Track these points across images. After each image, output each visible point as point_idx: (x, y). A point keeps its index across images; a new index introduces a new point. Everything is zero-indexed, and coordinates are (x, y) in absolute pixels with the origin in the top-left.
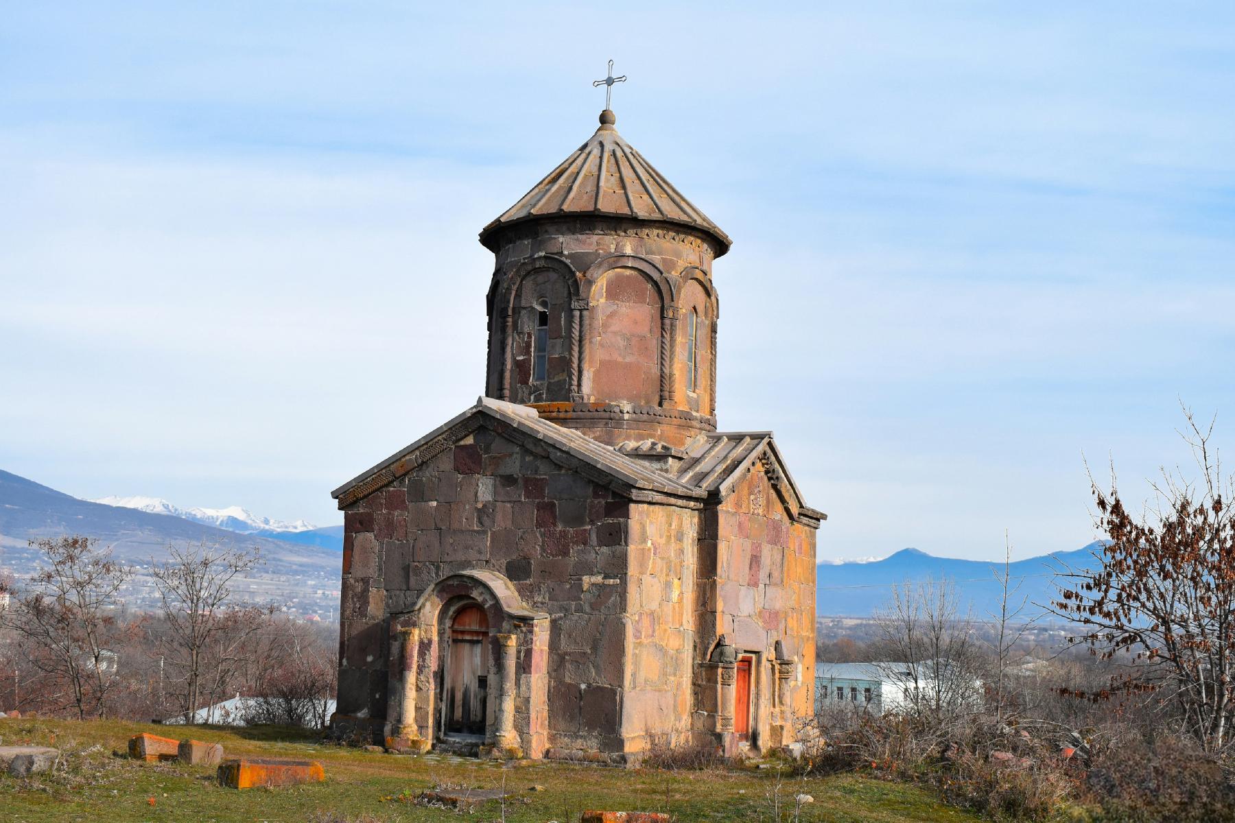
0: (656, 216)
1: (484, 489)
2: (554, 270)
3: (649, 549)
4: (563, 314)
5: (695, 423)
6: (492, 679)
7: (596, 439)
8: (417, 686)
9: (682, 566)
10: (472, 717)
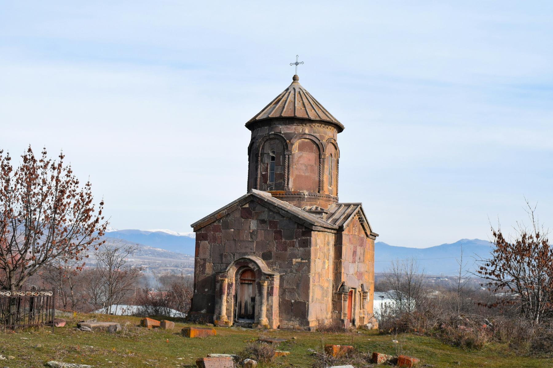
0: (318, 119)
1: (253, 225)
2: (278, 139)
3: (318, 249)
4: (281, 156)
5: (332, 199)
6: (257, 298)
7: (294, 205)
8: (227, 301)
9: (329, 255)
10: (248, 313)
